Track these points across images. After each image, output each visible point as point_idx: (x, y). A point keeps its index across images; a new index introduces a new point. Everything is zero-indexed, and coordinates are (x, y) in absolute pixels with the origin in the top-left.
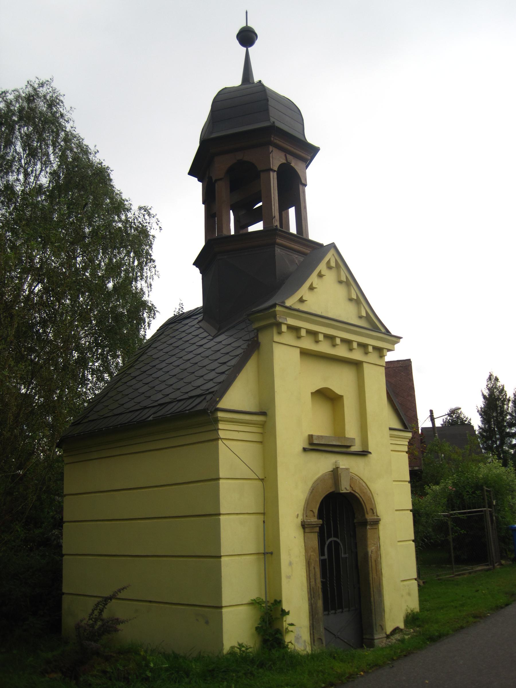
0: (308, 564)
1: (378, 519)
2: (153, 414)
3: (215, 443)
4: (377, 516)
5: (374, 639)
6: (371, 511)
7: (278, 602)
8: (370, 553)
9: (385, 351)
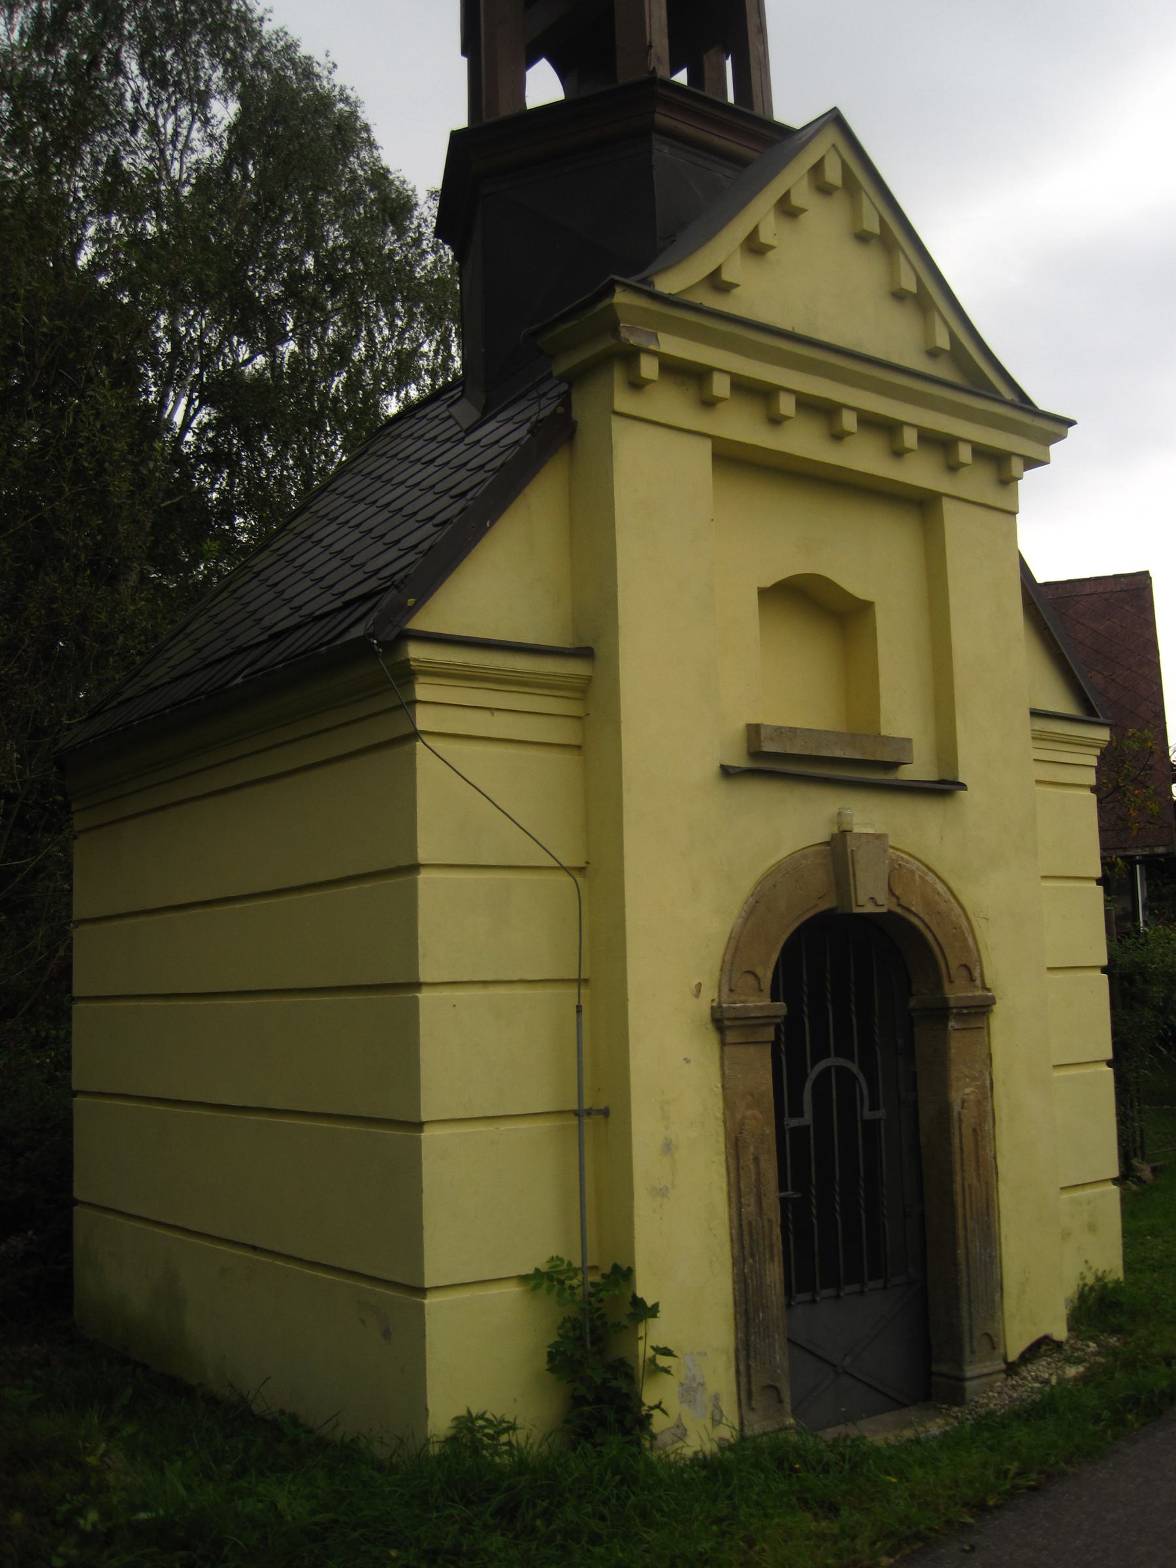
0: (735, 1146)
1: (987, 997)
2: (248, 666)
3: (406, 748)
4: (984, 988)
5: (963, 1379)
6: (964, 972)
7: (623, 1275)
8: (956, 1107)
9: (1016, 464)
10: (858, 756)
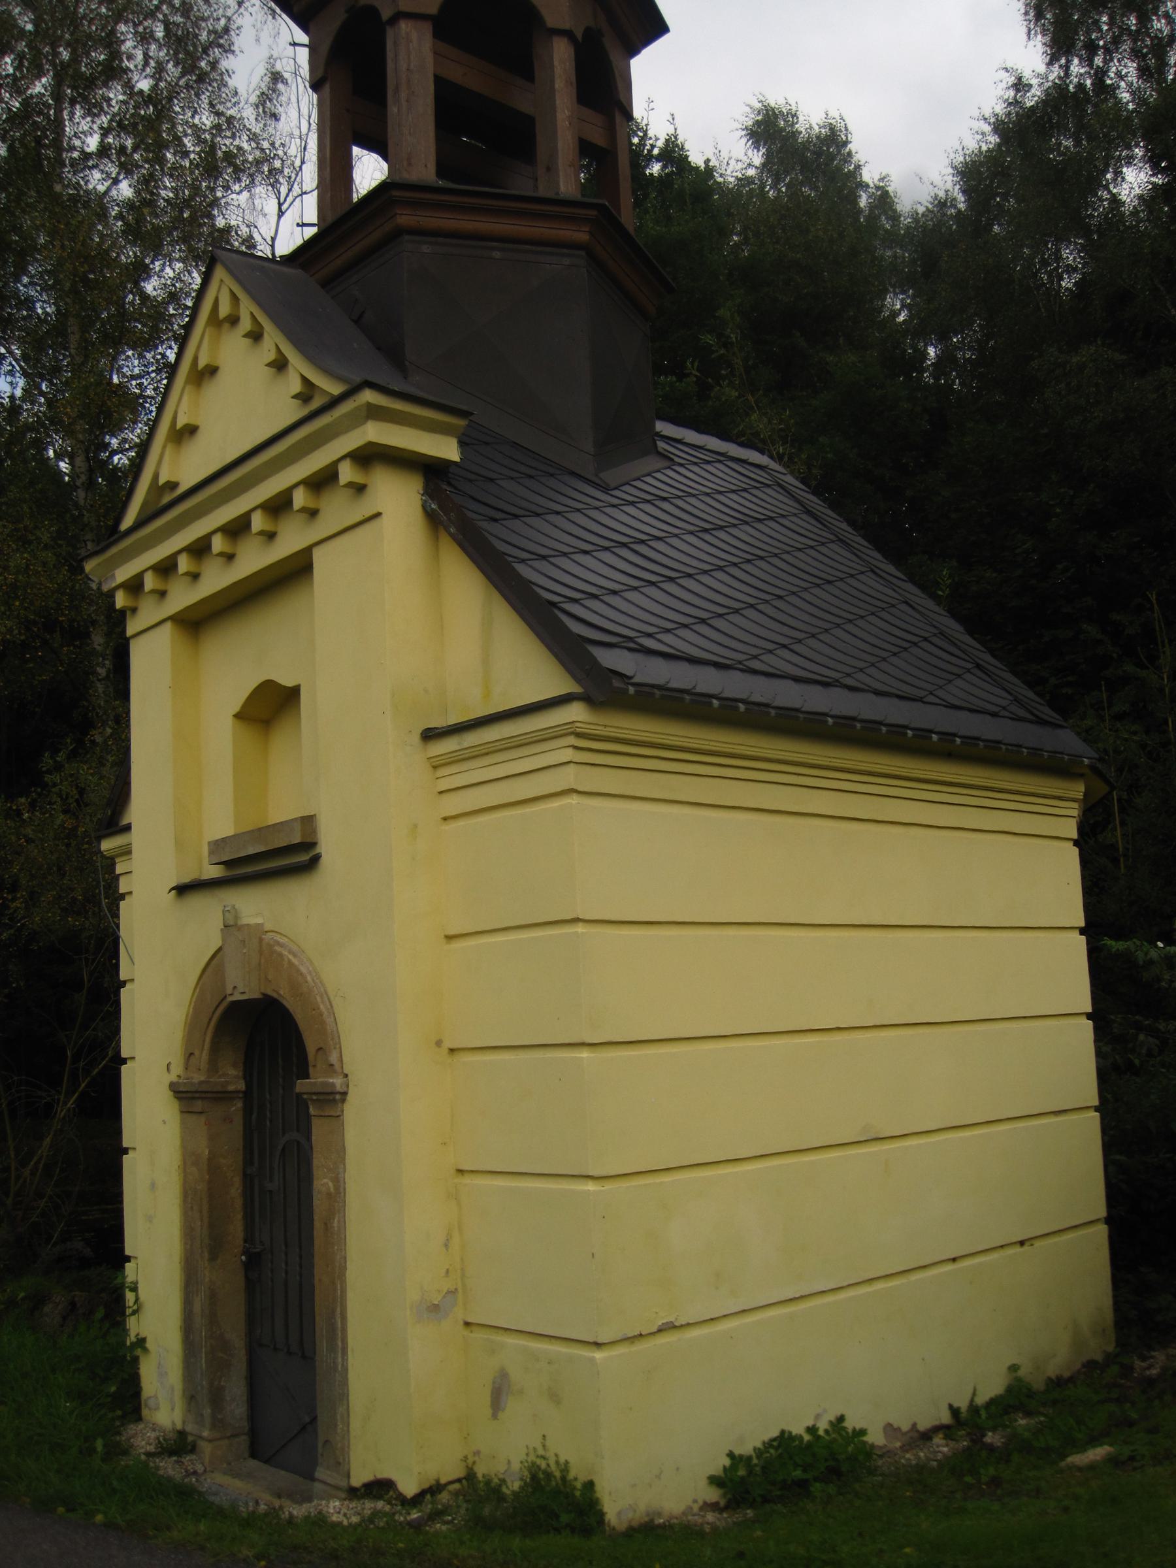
10: (262, 848)
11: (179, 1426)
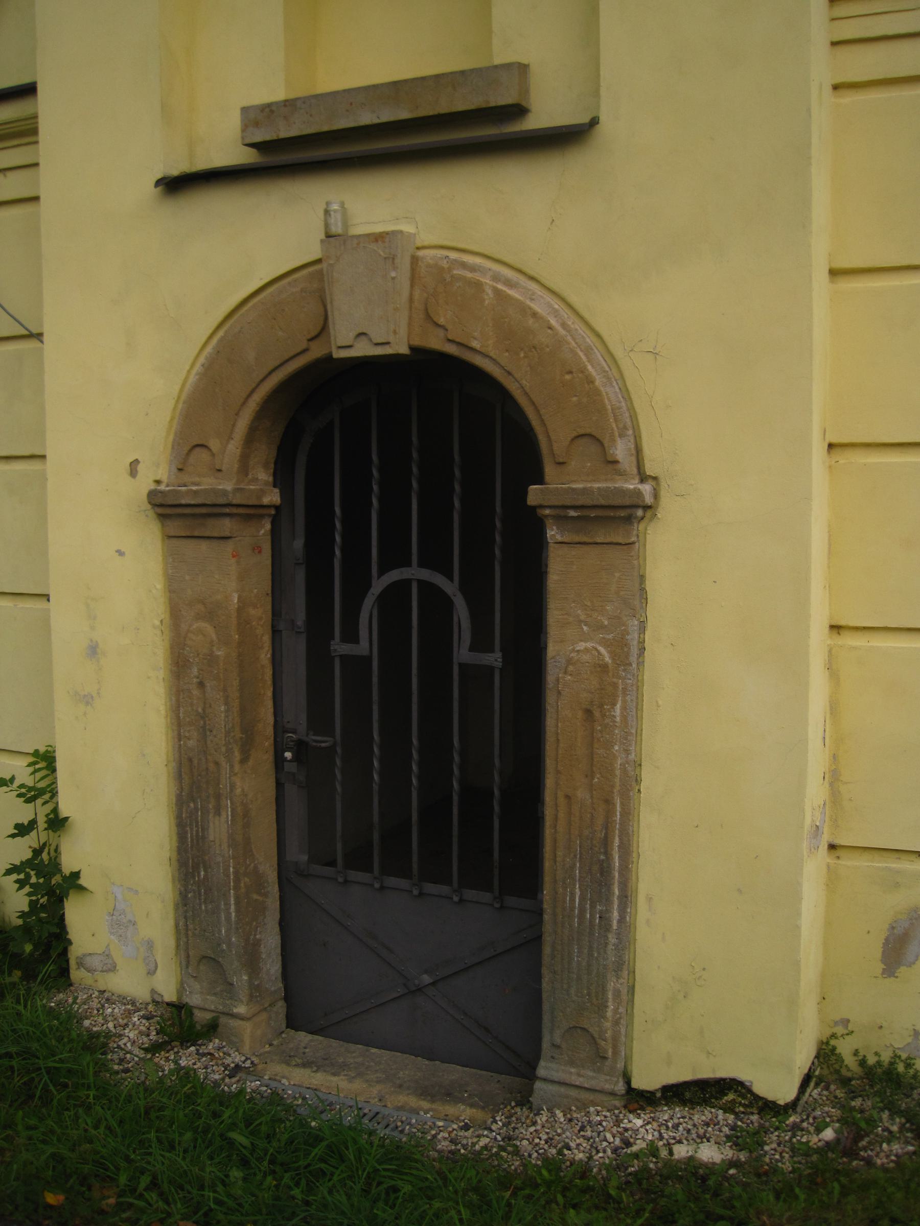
10: (404, 114)
11: (170, 995)
